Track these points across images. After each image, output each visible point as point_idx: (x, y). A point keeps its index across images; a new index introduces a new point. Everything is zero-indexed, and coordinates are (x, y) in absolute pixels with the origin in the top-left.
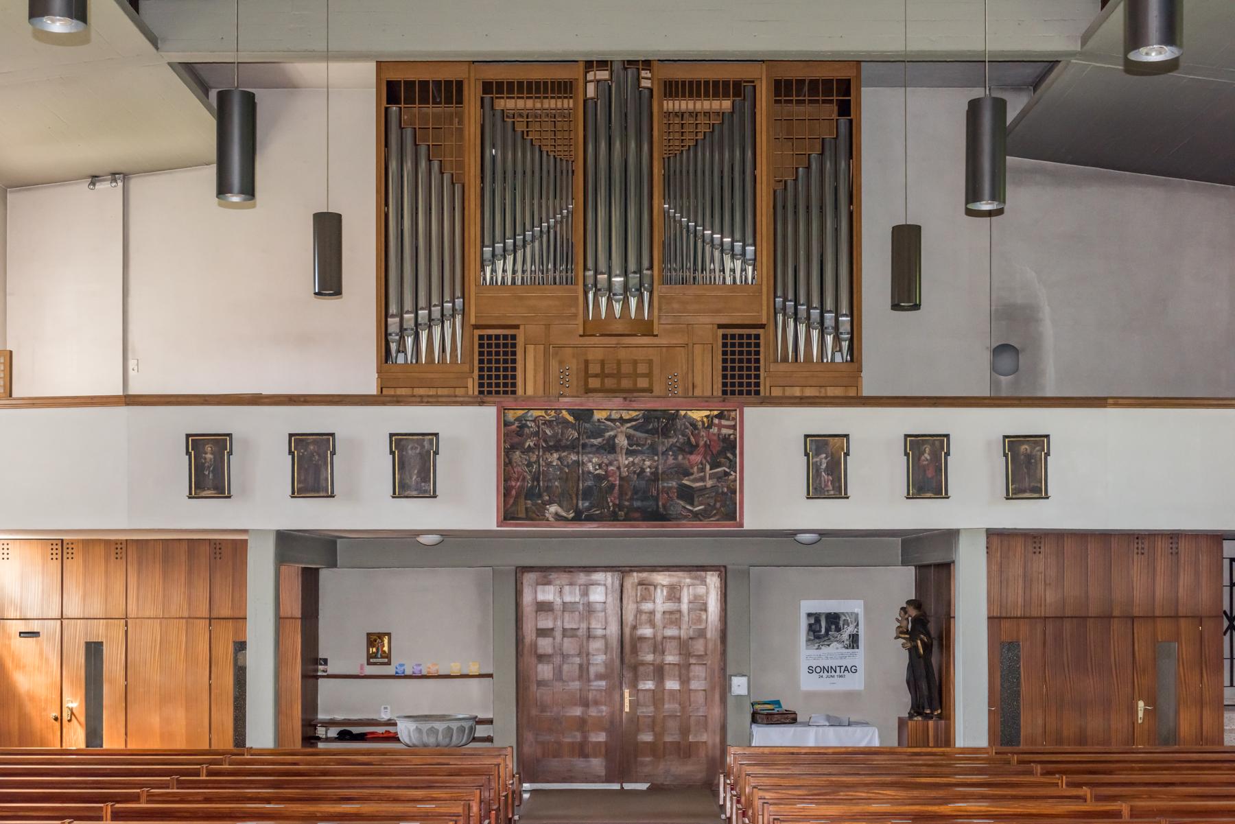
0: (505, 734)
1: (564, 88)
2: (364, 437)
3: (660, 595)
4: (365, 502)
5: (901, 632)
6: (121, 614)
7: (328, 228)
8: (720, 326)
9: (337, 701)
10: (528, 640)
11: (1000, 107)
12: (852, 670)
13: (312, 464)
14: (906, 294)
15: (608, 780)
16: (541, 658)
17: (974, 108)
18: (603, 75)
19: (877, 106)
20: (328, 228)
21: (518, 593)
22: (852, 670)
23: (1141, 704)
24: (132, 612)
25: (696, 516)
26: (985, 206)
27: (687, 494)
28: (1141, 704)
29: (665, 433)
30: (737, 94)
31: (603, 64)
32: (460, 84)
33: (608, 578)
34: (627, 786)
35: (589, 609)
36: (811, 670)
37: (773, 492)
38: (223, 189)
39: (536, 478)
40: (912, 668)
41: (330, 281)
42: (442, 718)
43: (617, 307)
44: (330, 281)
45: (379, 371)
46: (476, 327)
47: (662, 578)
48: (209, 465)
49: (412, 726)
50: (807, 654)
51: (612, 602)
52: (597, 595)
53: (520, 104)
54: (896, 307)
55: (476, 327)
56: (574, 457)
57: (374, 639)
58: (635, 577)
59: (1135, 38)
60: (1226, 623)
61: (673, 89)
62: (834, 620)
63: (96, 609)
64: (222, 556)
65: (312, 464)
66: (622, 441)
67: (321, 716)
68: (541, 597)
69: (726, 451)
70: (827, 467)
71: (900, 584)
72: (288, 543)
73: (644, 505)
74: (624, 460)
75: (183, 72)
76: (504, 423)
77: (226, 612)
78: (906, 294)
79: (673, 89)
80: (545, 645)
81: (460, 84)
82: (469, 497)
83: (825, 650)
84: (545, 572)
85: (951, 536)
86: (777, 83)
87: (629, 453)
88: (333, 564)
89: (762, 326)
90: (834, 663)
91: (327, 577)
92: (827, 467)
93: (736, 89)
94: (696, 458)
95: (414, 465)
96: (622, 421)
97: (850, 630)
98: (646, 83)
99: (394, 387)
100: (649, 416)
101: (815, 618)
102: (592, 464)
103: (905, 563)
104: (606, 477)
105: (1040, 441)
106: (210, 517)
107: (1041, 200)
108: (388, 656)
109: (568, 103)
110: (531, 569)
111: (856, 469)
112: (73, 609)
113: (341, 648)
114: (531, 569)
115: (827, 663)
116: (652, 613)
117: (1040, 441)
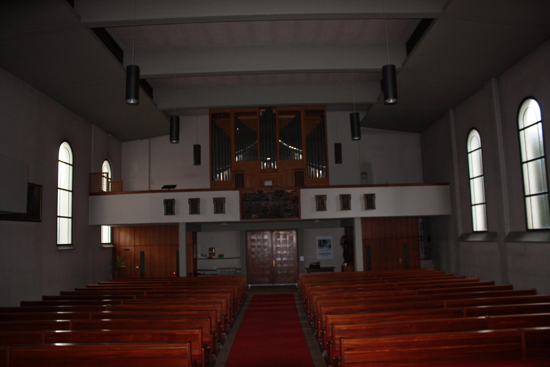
1: (255, 114)
2: (207, 199)
3: (281, 236)
4: (207, 215)
5: (341, 244)
7: (197, 149)
11: (358, 115)
12: (330, 254)
13: (194, 206)
14: (338, 159)
15: (270, 283)
16: (253, 253)
17: (352, 115)
18: (264, 110)
19: (330, 117)
20: (197, 149)
21: (246, 237)
22: (330, 254)
26: (356, 138)
28: (400, 260)
31: (263, 108)
33: (269, 233)
34: (275, 285)
35: (264, 240)
36: (320, 254)
37: (308, 210)
38: (171, 139)
41: (197, 161)
44: (197, 161)
45: (211, 183)
47: (281, 233)
50: (318, 250)
51: (270, 239)
52: (266, 237)
53: (244, 118)
56: (258, 202)
57: (211, 249)
58: (275, 232)
59: (386, 97)
60: (420, 239)
61: (281, 113)
65: (194, 206)
66: (270, 198)
69: (297, 200)
71: (341, 232)
72: (189, 225)
74: (271, 203)
75: (430, 17)
76: (241, 195)
78: (338, 159)
80: (253, 249)
82: (233, 213)
83: (323, 249)
84: (253, 232)
87: (272, 201)
88: (200, 231)
90: (325, 252)
91: (199, 234)
93: (297, 113)
95: (219, 206)
96: (271, 193)
97: (328, 244)
98: (274, 112)
99: (215, 186)
101: (320, 241)
103: (342, 226)
107: (371, 138)
109: (255, 117)
110: (249, 231)
112: (137, 243)
113: (201, 250)
114: (249, 231)
115: (323, 252)
116: (280, 241)
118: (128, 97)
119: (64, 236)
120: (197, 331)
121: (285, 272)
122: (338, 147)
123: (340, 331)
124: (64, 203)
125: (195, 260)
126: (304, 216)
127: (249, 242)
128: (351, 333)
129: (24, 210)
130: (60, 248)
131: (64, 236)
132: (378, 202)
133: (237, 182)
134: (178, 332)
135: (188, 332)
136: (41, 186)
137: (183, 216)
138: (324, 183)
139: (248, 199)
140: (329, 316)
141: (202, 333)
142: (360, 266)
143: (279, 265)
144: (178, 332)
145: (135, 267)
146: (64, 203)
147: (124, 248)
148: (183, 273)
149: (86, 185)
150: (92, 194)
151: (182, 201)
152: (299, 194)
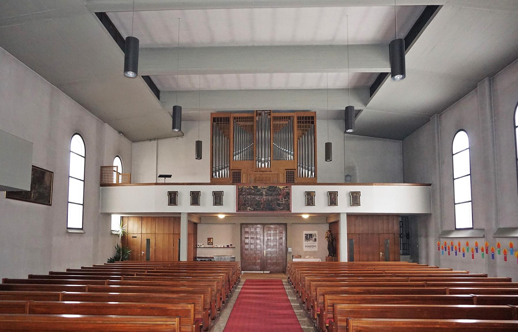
0: (238, 259)
2: (207, 192)
4: (207, 206)
6: (154, 232)
7: (199, 145)
8: (286, 170)
9: (201, 253)
10: (243, 239)
13: (195, 198)
14: (328, 157)
16: (246, 255)
20: (199, 145)
23: (381, 253)
24: (157, 232)
25: (281, 210)
27: (279, 205)
28: (381, 253)
29: (274, 191)
30: (289, 119)
32: (229, 118)
39: (245, 201)
40: (329, 245)
41: (199, 156)
42: (224, 256)
43: (263, 165)
44: (199, 156)
46: (232, 170)
48: (173, 198)
49: (217, 257)
50: (305, 243)
54: (326, 160)
55: (232, 170)
57: (209, 239)
58: (267, 226)
62: (311, 235)
63: (149, 232)
64: (176, 218)
65: (195, 198)
66: (264, 193)
67: (198, 256)
68: (246, 236)
69: (288, 195)
70: (310, 198)
73: (269, 207)
74: (264, 197)
77: (177, 232)
78: (328, 157)
79: (275, 118)
81: (229, 118)
82: (230, 204)
85: (338, 215)
86: (298, 117)
87: (266, 196)
89: (295, 169)
92: (310, 198)
94: (280, 197)
95: (218, 198)
96: (264, 188)
99: (214, 182)
100: (270, 187)
102: (257, 198)
104: (260, 201)
105: (358, 193)
106: (173, 209)
108: (212, 243)
111: (317, 199)
112: (144, 232)
113: (202, 242)
117: (358, 193)
118: (126, 70)
119: (75, 218)
120: (190, 307)
121: (274, 261)
122: (328, 146)
123: (342, 313)
124: (76, 191)
125: (196, 247)
126: (293, 211)
127: (243, 233)
128: (358, 314)
129: (27, 188)
130: (70, 231)
131: (75, 218)
132: (362, 199)
133: (235, 178)
134: (170, 307)
135: (180, 307)
136: (53, 173)
137: (184, 207)
138: (314, 182)
139: (244, 193)
140: (327, 297)
141: (195, 310)
142: (344, 256)
143: (270, 255)
144: (170, 307)
145: (141, 253)
146: (76, 191)
147: (132, 235)
148: (184, 258)
149: (100, 179)
150: (102, 185)
151: (184, 194)
152: (290, 190)
